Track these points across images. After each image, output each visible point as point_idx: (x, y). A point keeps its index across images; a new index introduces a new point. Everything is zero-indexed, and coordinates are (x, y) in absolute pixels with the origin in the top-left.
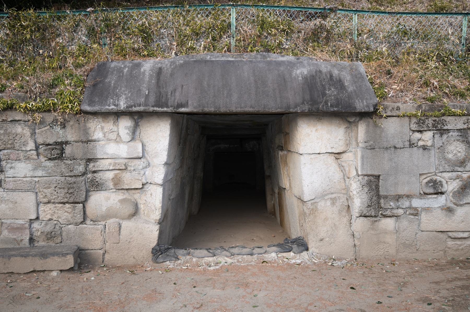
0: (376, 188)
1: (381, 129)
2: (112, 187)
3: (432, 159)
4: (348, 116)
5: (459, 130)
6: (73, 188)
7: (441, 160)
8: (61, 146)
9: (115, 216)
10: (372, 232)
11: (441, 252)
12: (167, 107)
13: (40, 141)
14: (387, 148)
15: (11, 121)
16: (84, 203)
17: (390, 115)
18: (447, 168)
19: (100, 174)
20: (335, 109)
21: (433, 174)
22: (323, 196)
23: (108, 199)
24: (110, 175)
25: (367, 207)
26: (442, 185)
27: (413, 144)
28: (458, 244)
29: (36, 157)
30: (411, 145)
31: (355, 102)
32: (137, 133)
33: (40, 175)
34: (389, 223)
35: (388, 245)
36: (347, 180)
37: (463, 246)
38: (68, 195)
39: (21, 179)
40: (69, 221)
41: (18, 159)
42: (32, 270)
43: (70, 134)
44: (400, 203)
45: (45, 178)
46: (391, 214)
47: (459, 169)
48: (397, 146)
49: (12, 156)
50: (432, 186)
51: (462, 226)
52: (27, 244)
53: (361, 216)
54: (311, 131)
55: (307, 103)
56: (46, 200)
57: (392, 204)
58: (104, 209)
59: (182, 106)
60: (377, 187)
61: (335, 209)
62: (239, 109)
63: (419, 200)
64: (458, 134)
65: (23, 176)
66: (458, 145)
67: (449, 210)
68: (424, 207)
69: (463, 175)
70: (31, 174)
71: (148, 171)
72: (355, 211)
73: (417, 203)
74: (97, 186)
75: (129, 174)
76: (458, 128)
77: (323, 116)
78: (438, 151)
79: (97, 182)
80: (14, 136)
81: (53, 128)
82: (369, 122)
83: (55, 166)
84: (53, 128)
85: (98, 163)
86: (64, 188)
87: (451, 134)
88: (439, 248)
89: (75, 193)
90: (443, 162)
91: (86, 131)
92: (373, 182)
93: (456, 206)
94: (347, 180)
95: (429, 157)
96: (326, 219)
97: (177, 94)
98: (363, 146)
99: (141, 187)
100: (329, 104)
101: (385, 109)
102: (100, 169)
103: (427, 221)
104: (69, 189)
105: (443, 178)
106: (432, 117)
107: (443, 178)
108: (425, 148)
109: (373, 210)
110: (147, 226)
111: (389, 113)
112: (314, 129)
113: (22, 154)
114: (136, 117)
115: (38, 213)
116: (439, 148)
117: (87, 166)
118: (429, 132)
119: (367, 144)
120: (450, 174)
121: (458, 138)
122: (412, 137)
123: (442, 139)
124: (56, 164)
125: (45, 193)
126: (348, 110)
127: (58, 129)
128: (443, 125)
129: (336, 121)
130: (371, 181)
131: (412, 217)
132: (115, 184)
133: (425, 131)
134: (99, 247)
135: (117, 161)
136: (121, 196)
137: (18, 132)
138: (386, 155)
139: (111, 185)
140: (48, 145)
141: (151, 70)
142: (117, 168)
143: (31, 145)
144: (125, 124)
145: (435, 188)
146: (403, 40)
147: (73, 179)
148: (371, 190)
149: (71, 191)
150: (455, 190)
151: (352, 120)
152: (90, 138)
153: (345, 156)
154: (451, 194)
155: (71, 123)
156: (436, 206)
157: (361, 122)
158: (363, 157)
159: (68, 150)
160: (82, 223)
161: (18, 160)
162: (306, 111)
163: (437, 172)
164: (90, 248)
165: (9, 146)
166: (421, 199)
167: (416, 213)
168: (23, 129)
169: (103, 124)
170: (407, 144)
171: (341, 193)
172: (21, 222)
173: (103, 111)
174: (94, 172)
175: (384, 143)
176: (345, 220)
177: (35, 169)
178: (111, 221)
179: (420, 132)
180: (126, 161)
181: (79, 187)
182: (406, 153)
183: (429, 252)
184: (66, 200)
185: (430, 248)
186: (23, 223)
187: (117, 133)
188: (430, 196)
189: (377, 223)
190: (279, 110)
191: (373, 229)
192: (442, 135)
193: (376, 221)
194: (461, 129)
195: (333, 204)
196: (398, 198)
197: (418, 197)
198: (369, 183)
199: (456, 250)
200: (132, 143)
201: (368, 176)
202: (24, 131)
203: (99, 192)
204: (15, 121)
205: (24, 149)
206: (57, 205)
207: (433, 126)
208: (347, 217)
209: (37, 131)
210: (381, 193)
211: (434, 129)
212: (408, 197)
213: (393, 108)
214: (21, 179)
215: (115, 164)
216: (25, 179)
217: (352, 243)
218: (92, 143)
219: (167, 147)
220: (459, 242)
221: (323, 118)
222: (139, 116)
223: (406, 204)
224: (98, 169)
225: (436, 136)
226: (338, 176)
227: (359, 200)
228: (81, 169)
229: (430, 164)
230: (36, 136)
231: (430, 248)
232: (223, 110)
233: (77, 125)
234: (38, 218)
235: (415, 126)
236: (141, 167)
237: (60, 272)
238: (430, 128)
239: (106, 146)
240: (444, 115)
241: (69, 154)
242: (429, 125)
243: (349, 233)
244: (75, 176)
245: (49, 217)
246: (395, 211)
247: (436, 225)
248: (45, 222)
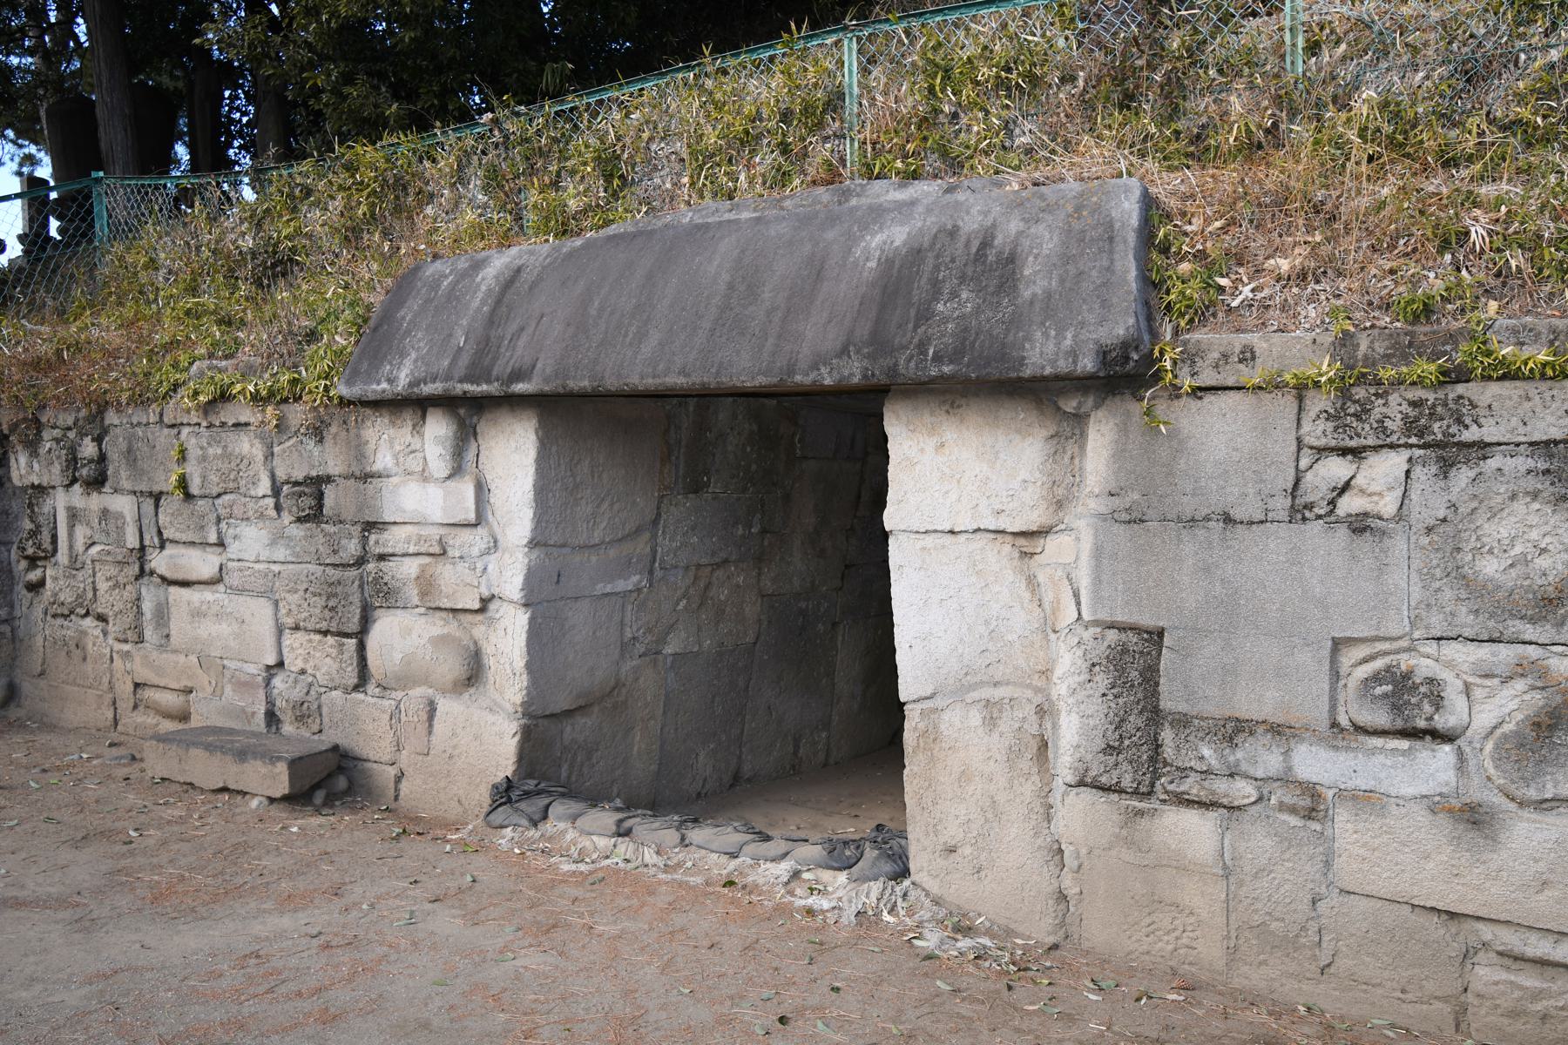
0: (1146, 680)
1: (1174, 443)
2: (416, 601)
3: (1397, 577)
4: (1062, 392)
5: (1545, 447)
6: (335, 595)
7: (1438, 584)
8: (316, 485)
9: (425, 681)
10: (1128, 855)
11: (1438, 1005)
12: (489, 382)
13: (281, 474)
14: (1193, 520)
15: (235, 425)
16: (361, 634)
17: (1213, 383)
18: (1468, 622)
20: (946, 369)
21: (1404, 643)
22: (961, 690)
23: (408, 631)
25: (1104, 751)
26: (1438, 701)
27: (1309, 506)
28: (1521, 988)
29: (273, 513)
30: (1299, 512)
31: (1027, 338)
32: (470, 455)
34: (1190, 832)
35: (1192, 919)
36: (1053, 636)
37: (1552, 1002)
38: (327, 614)
40: (332, 680)
42: (221, 785)
43: (330, 458)
44: (1239, 754)
45: (291, 566)
46: (1204, 796)
47: (1530, 632)
48: (1237, 514)
50: (1385, 695)
51: (1543, 906)
52: (262, 727)
53: (1081, 783)
54: (922, 450)
55: (858, 352)
57: (1206, 752)
58: (398, 656)
59: (518, 375)
60: (1150, 676)
61: (998, 743)
62: (650, 381)
63: (1324, 754)
64: (1530, 463)
66: (1534, 519)
67: (1473, 818)
68: (1350, 785)
69: (1554, 662)
70: (264, 556)
71: (492, 562)
72: (1064, 764)
73: (1315, 763)
75: (449, 567)
76: (1536, 437)
77: (964, 395)
78: (1425, 541)
82: (1128, 414)
83: (305, 537)
85: (386, 535)
87: (1492, 464)
88: (1430, 986)
89: (340, 609)
90: (1448, 594)
91: (359, 451)
92: (1135, 662)
93: (1512, 806)
95: (1382, 568)
96: (965, 776)
97: (521, 343)
98: (1103, 510)
99: (477, 606)
100: (931, 352)
101: (1190, 357)
102: (390, 551)
103: (1367, 854)
105: (1450, 665)
106: (1411, 387)
107: (1450, 665)
108: (1360, 525)
109: (1125, 766)
110: (491, 718)
111: (1208, 378)
112: (930, 443)
114: (462, 412)
115: (280, 653)
116: (1429, 530)
117: (364, 541)
118: (1392, 454)
119: (1116, 502)
120: (1484, 652)
121: (1532, 483)
122: (1309, 476)
123: (1447, 489)
126: (994, 372)
127: (311, 444)
128: (1459, 421)
129: (1022, 413)
130: (1125, 651)
131: (1294, 821)
132: (423, 594)
133: (1376, 449)
134: (386, 758)
135: (425, 531)
136: (437, 627)
138: (1188, 548)
139: (413, 594)
140: (296, 484)
141: (496, 277)
142: (423, 550)
143: (264, 486)
144: (438, 428)
145: (1397, 708)
146: (1522, 36)
148: (1120, 683)
149: (331, 604)
150: (1508, 727)
151: (1069, 405)
152: (368, 469)
153: (1052, 543)
154: (1489, 746)
155: (333, 429)
156: (1409, 791)
157: (1100, 413)
158: (1098, 553)
160: (356, 688)
162: (856, 380)
163: (1416, 635)
164: (371, 757)
166: (1336, 748)
167: (1312, 804)
170: (1282, 504)
171: (1028, 686)
173: (371, 397)
174: (382, 557)
175: (1185, 499)
176: (1028, 789)
178: (419, 692)
179: (1356, 453)
180: (443, 531)
182: (1278, 541)
183: (1380, 991)
184: (324, 626)
185: (1386, 974)
188: (1378, 742)
189: (1144, 822)
190: (761, 380)
191: (1130, 843)
192: (1446, 467)
193: (1140, 813)
194: (1556, 442)
195: (991, 722)
196: (1234, 730)
197: (1320, 740)
198: (1118, 660)
199: (1514, 1014)
200: (451, 484)
201: (1122, 628)
203: (392, 611)
205: (253, 493)
206: (312, 636)
207: (1410, 426)
208: (1036, 778)
209: (276, 449)
210: (1166, 704)
211: (1413, 440)
212: (1278, 731)
213: (1225, 356)
215: (420, 539)
216: (257, 566)
217: (1048, 887)
218: (375, 481)
219: (531, 495)
220: (1530, 980)
221: (963, 401)
222: (469, 411)
223: (1268, 760)
225: (1418, 471)
226: (1021, 621)
227: (1075, 718)
228: (352, 548)
229: (1388, 597)
231: (1386, 974)
232: (611, 383)
234: (280, 664)
235: (1322, 425)
236: (475, 551)
237: (266, 802)
238: (1394, 438)
239: (401, 490)
240: (1459, 375)
242: (1388, 423)
243: (1039, 841)
244: (343, 565)
245: (300, 664)
246: (1221, 786)
247: (1406, 876)
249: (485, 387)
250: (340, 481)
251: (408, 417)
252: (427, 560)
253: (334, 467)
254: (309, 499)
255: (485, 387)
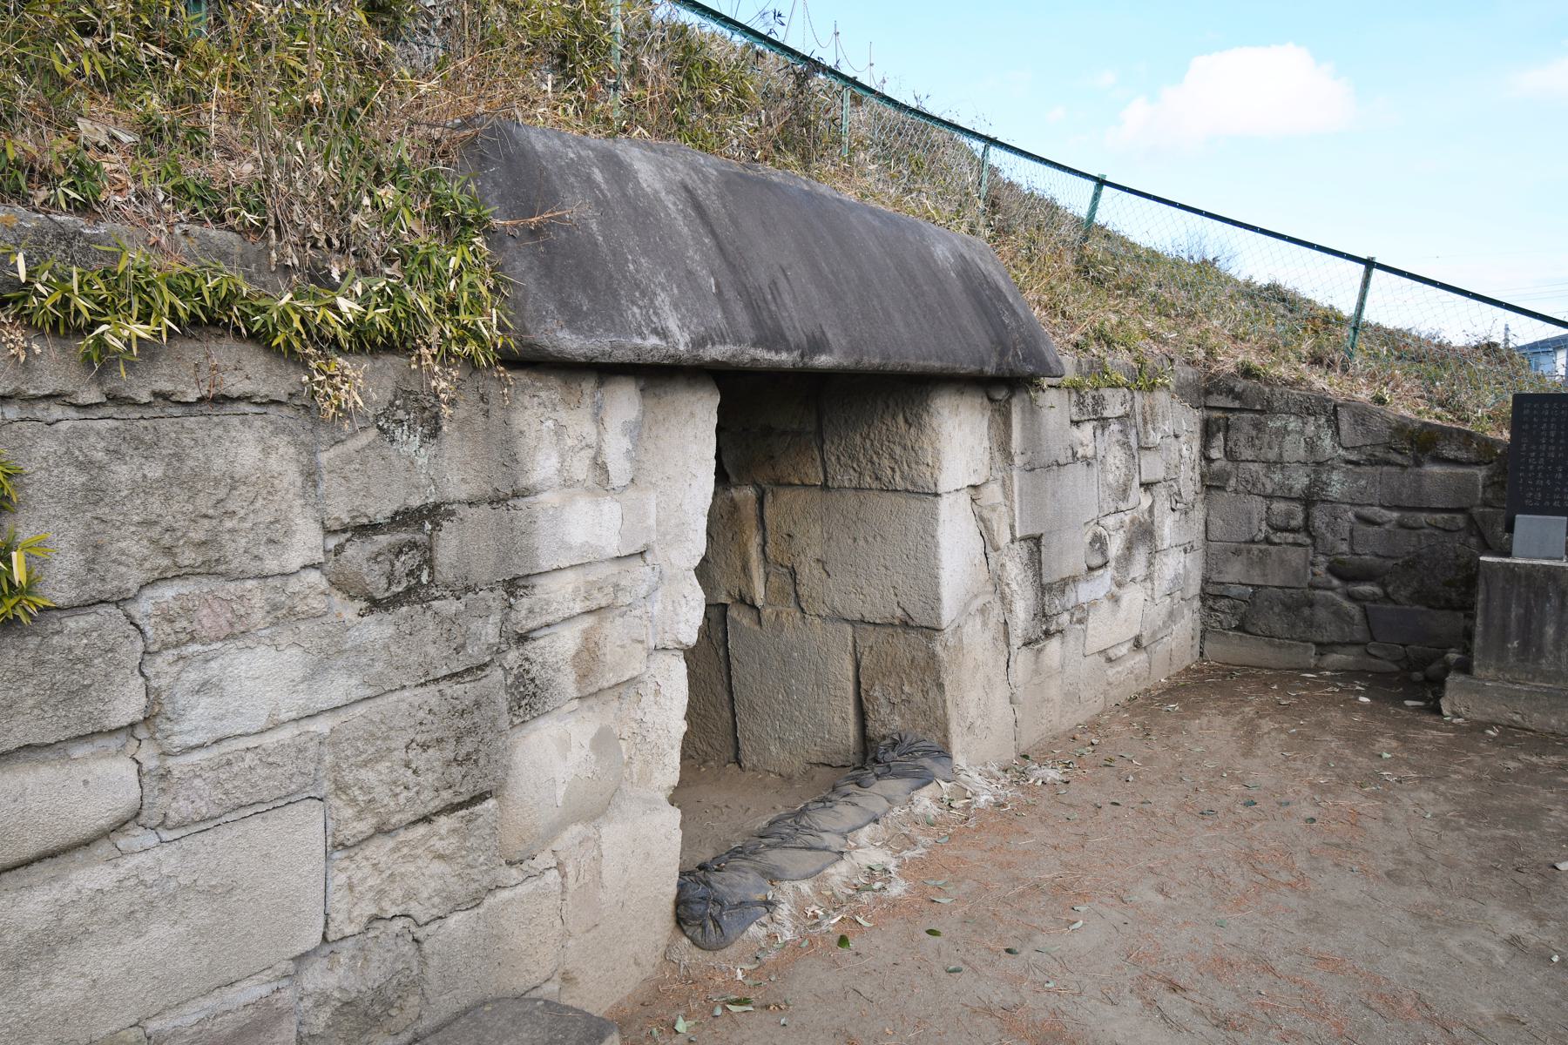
12: (789, 350)
19: (541, 642)
24: (567, 641)
33: (338, 698)
38: (457, 772)
39: (252, 742)
41: (239, 628)
43: (447, 469)
45: (360, 709)
49: (207, 620)
56: (365, 826)
61: (988, 636)
65: (262, 723)
74: (528, 697)
79: (533, 680)
80: (222, 492)
81: (392, 441)
83: (399, 636)
84: (392, 441)
86: (440, 741)
91: (509, 456)
94: (991, 555)
104: (458, 740)
113: (258, 600)
124: (405, 628)
125: (370, 790)
127: (410, 443)
137: (239, 472)
147: (463, 691)
149: (469, 745)
159: (449, 545)
161: (237, 633)
165: (188, 557)
168: (266, 451)
169: (563, 415)
172: (253, 990)
177: (317, 671)
181: (494, 720)
186: (264, 990)
187: (591, 452)
202: (273, 463)
203: (530, 726)
204: (222, 400)
205: (271, 565)
214: (252, 742)
216: (269, 740)
224: (550, 619)
230: (322, 487)
233: (480, 419)
241: (452, 566)
248: (349, 943)
249: (784, 356)
250: (463, 511)
251: (588, 386)
252: (589, 621)
253: (458, 483)
254: (401, 560)
255: (784, 356)
